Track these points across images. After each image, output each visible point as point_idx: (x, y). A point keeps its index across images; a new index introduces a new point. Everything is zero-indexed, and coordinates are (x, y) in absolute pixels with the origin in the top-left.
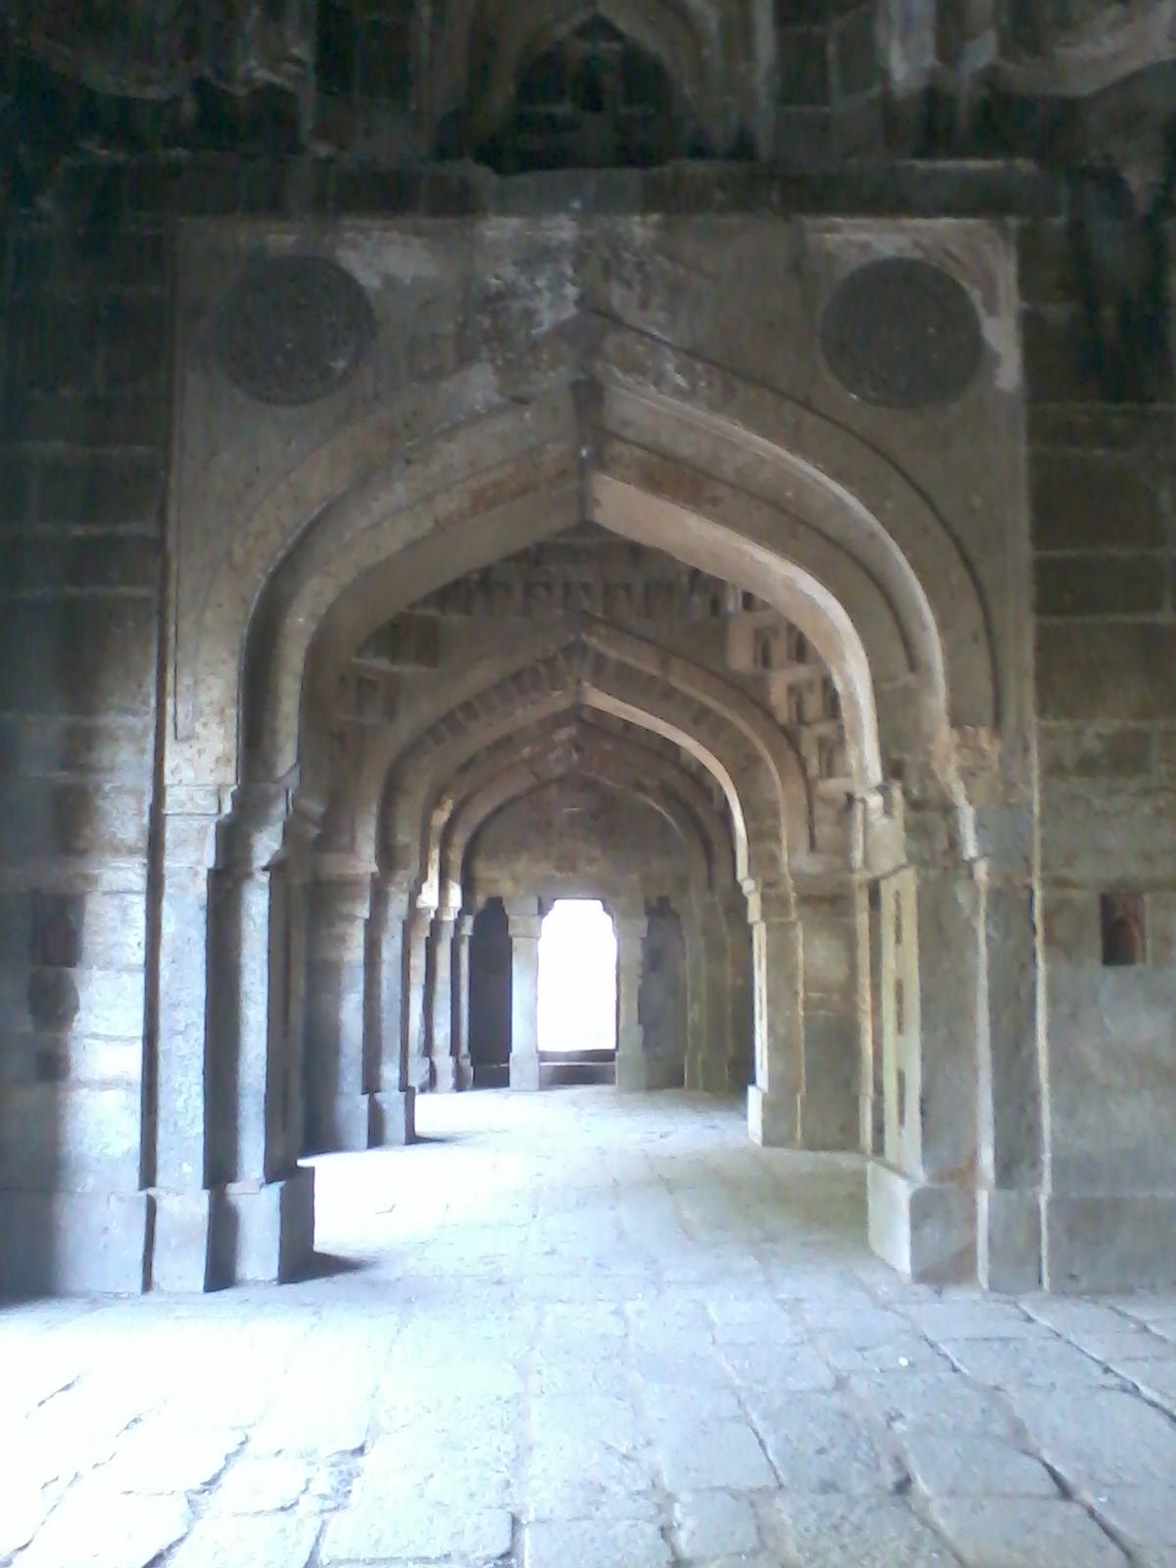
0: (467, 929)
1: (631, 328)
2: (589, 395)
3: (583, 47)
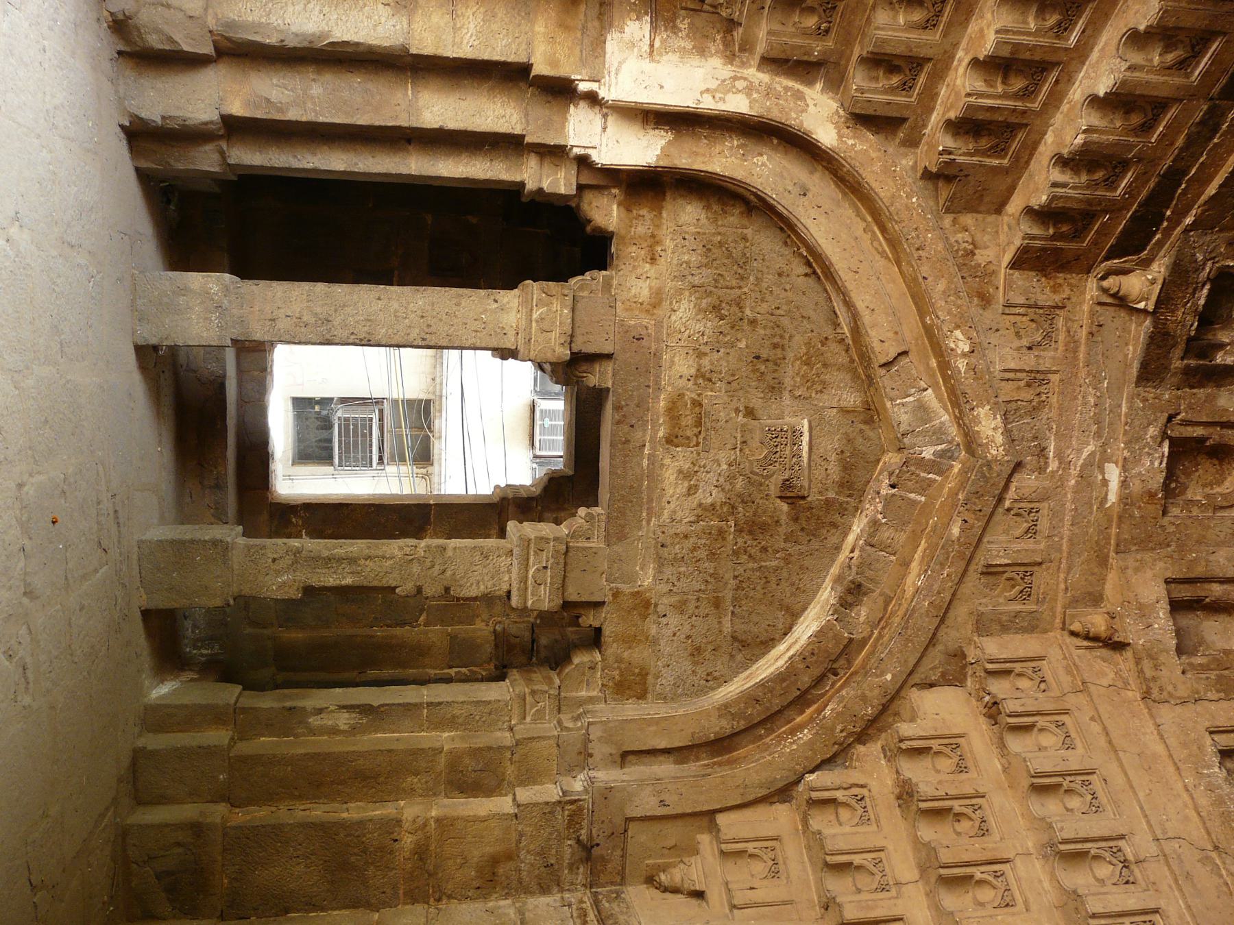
0: (535, 176)
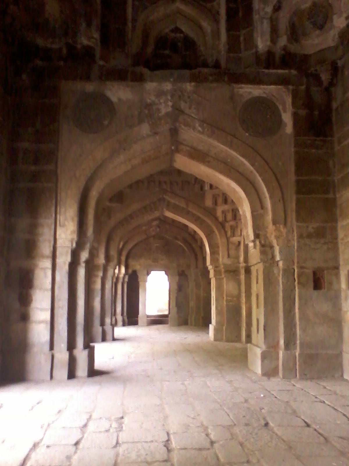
0: (126, 279)
1: (186, 114)
2: (174, 132)
3: (173, 35)
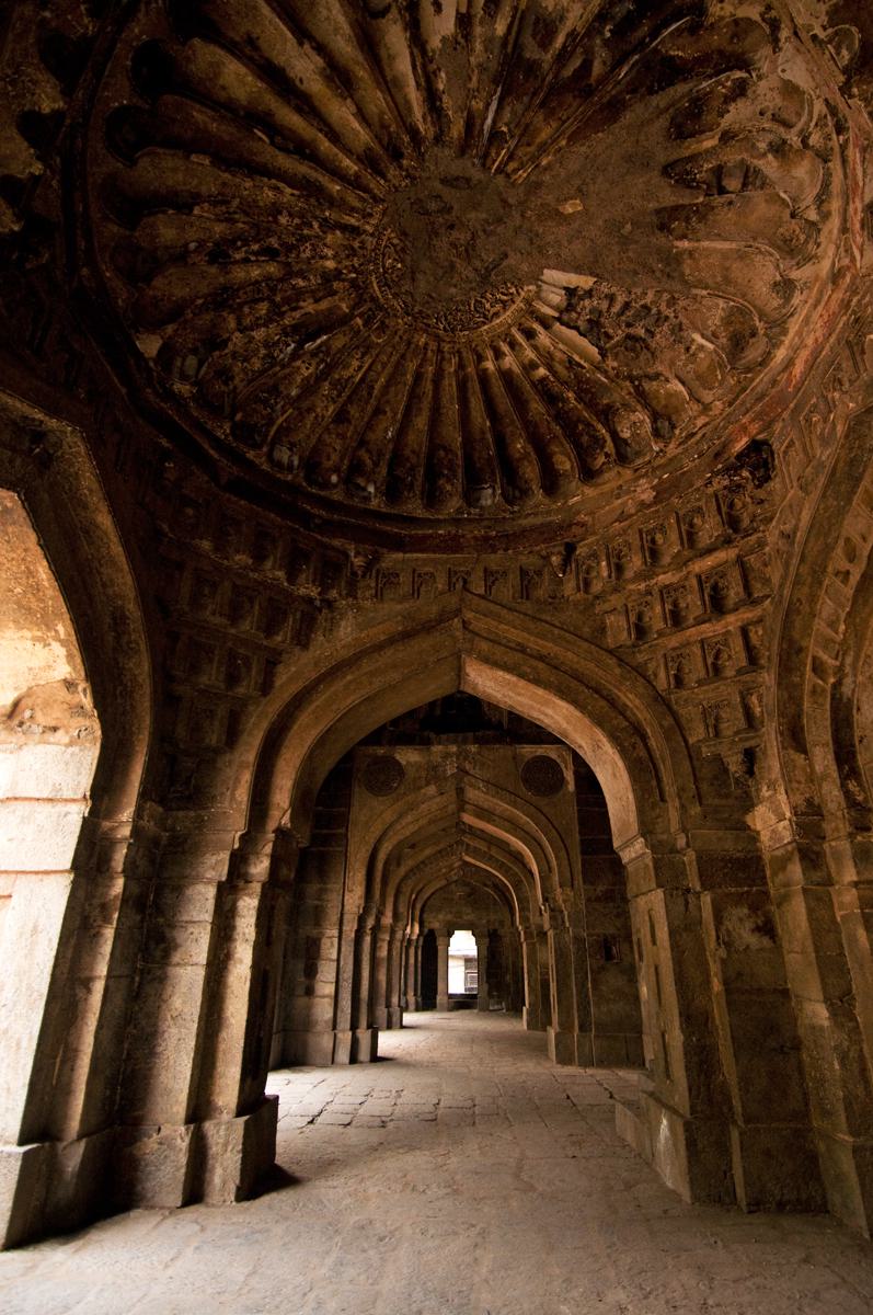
0: (421, 943)
2: (460, 791)
